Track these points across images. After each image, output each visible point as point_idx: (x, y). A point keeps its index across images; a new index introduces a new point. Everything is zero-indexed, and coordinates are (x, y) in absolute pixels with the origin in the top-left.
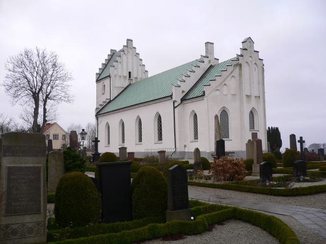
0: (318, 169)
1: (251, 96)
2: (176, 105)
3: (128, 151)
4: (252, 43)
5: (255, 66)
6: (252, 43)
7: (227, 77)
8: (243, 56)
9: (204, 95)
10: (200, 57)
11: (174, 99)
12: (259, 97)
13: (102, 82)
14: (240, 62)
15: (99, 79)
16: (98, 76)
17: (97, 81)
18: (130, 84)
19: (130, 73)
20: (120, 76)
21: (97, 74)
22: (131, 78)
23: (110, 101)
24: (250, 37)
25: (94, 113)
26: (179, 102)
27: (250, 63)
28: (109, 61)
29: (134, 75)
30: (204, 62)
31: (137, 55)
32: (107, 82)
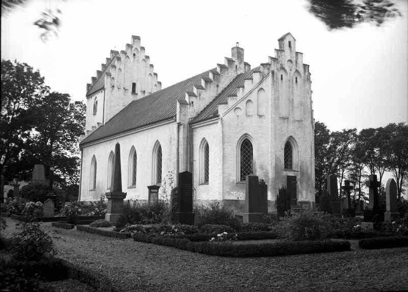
11: (178, 121)
13: (93, 98)
32: (100, 96)
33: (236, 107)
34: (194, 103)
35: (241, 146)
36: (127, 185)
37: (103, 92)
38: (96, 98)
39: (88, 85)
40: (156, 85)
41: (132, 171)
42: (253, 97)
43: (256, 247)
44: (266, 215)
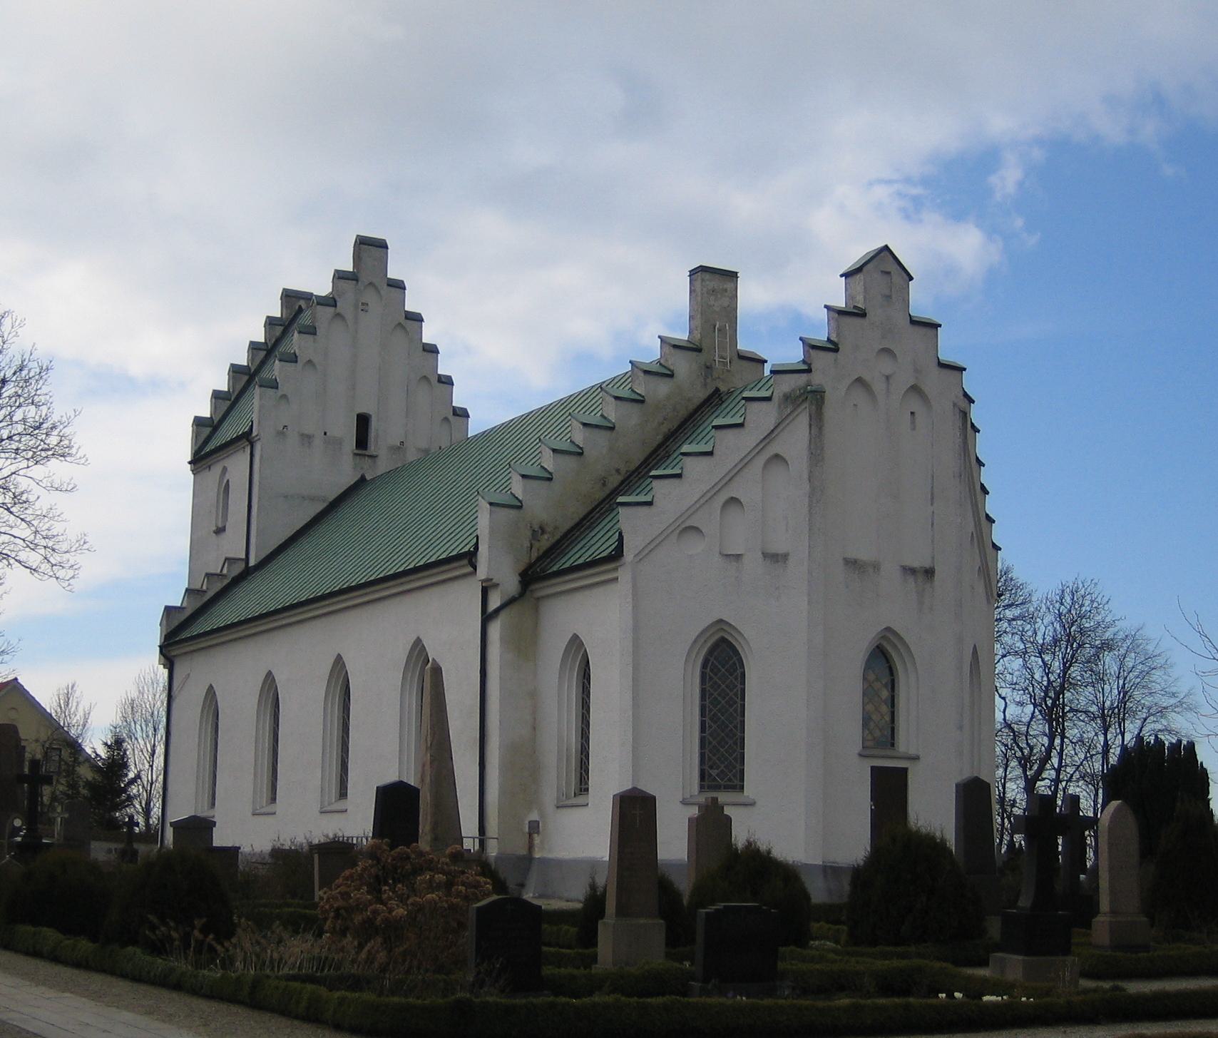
0: (44, 841)
1: (876, 567)
2: (494, 603)
3: (220, 838)
4: (897, 277)
5: (915, 404)
6: (897, 277)
7: (745, 463)
8: (836, 350)
9: (617, 554)
10: (656, 355)
11: (482, 572)
12: (929, 573)
13: (217, 469)
14: (817, 379)
15: (207, 449)
16: (207, 431)
17: (200, 459)
18: (362, 480)
19: (363, 422)
20: (307, 439)
21: (199, 422)
22: (372, 449)
23: (247, 573)
24: (886, 248)
25: (154, 637)
26: (510, 584)
27: (879, 387)
28: (264, 352)
29: (384, 434)
30: (671, 376)
31: (410, 325)
32: (237, 465)
33: (688, 524)
34: (916, 415)
35: (704, 666)
36: (851, 733)
37: (248, 450)
38: (225, 469)
39: (199, 422)
40: (446, 419)
41: (267, 744)
42: (747, 489)
43: (1166, 995)
44: (394, 879)
